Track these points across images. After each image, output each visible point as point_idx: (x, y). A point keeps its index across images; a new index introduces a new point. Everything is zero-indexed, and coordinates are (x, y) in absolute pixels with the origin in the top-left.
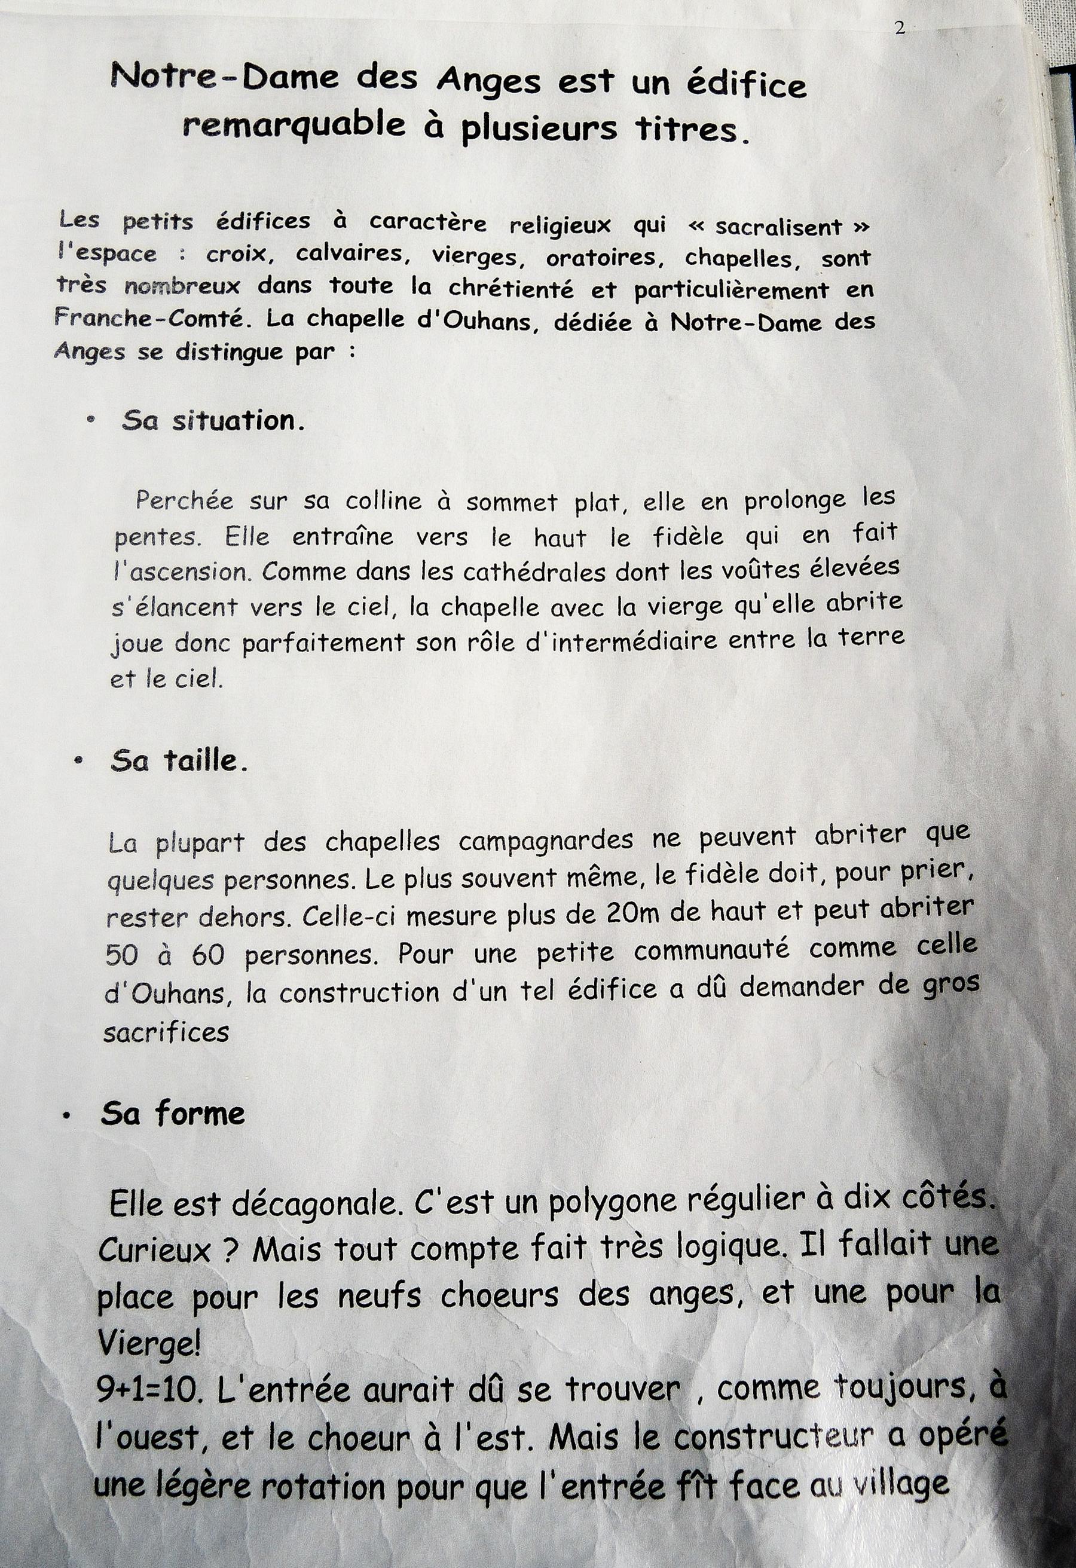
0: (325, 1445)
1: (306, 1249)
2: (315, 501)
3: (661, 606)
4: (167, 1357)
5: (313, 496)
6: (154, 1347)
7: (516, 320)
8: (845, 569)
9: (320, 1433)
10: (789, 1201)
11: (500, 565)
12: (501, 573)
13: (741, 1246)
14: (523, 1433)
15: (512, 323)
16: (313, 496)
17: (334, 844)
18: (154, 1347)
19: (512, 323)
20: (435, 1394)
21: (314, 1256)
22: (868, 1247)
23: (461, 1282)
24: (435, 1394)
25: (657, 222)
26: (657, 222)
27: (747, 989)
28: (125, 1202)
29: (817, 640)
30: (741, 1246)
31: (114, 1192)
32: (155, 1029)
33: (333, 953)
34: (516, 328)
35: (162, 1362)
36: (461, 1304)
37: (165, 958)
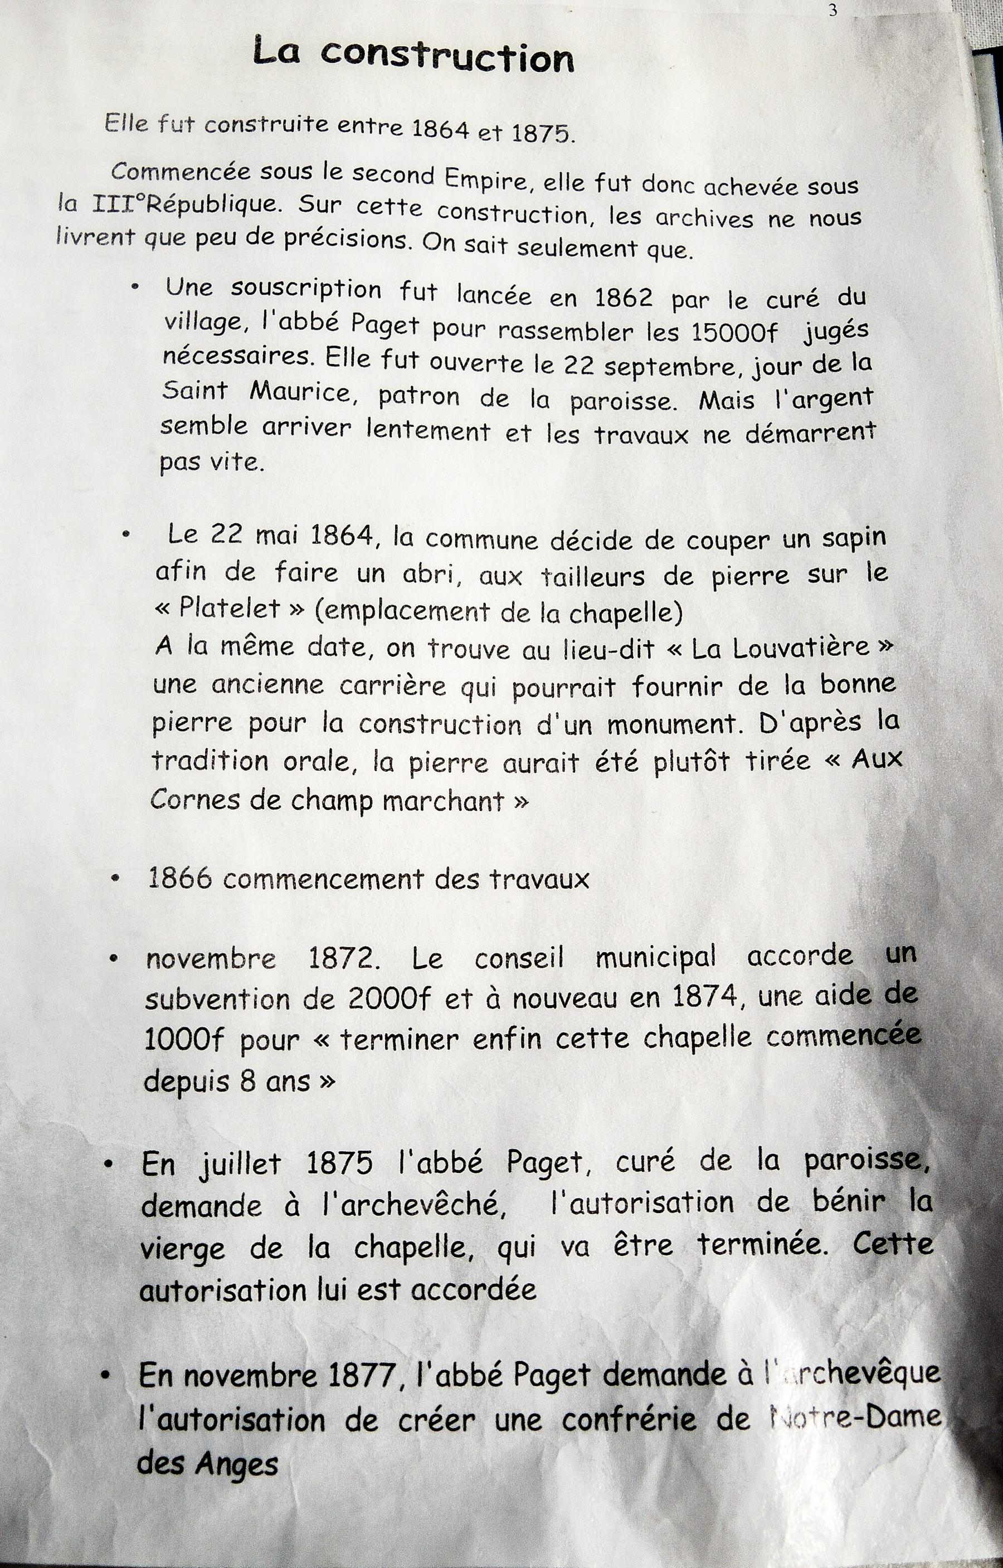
1: (215, 1080)
4: (201, 1261)
6: (188, 1252)
7: (384, 49)
8: (758, 189)
10: (460, 1423)
13: (509, 1248)
14: (399, 1285)
15: (379, 54)
17: (364, 1250)
18: (188, 1252)
19: (379, 54)
21: (223, 1087)
23: (372, 1235)
25: (487, 684)
26: (487, 684)
27: (652, 542)
28: (156, 1162)
29: (661, 542)
30: (509, 1248)
31: (146, 1153)
34: (385, 63)
35: (196, 1265)
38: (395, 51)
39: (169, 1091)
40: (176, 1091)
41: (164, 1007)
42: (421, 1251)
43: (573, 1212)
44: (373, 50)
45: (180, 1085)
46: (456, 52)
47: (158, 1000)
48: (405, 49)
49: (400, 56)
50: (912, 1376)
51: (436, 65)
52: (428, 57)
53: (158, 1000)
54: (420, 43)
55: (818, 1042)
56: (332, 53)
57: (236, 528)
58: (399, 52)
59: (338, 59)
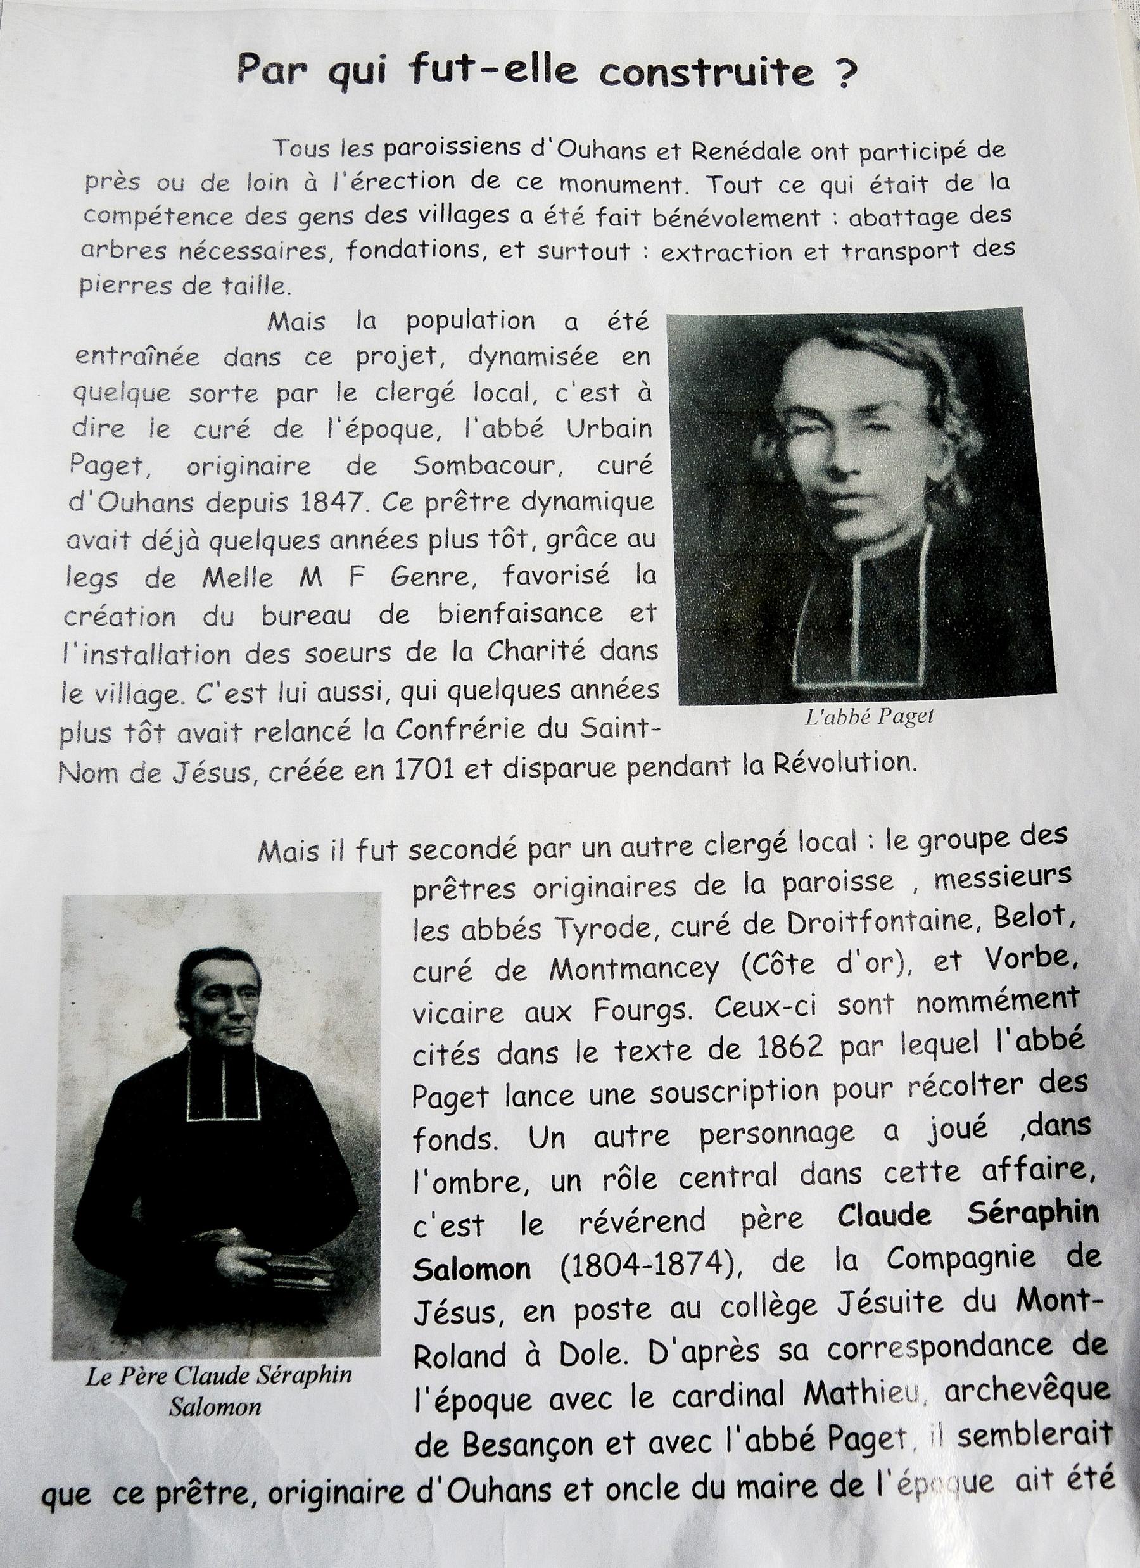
0: (992, 1396)
2: (542, 614)
3: (427, 1012)
5: (540, 609)
9: (987, 1386)
11: (858, 1383)
12: (858, 1394)
16: (540, 609)
20: (1036, 1484)
22: (1028, 1482)
24: (1036, 1484)
32: (546, 648)
33: (604, 687)
34: (665, 83)
36: (995, 1398)
37: (311, 185)
38: (675, 71)
39: (443, 1411)
40: (451, 1411)
41: (470, 1321)
42: (78, 1498)
43: (529, 1364)
44: (652, 70)
45: (454, 1404)
46: (738, 68)
47: (464, 1314)
48: (686, 68)
49: (680, 76)
50: (503, 1405)
51: (717, 83)
52: (709, 74)
53: (464, 1314)
54: (701, 61)
55: (970, 1008)
56: (611, 75)
57: (816, 1039)
58: (682, 81)
59: (618, 82)
